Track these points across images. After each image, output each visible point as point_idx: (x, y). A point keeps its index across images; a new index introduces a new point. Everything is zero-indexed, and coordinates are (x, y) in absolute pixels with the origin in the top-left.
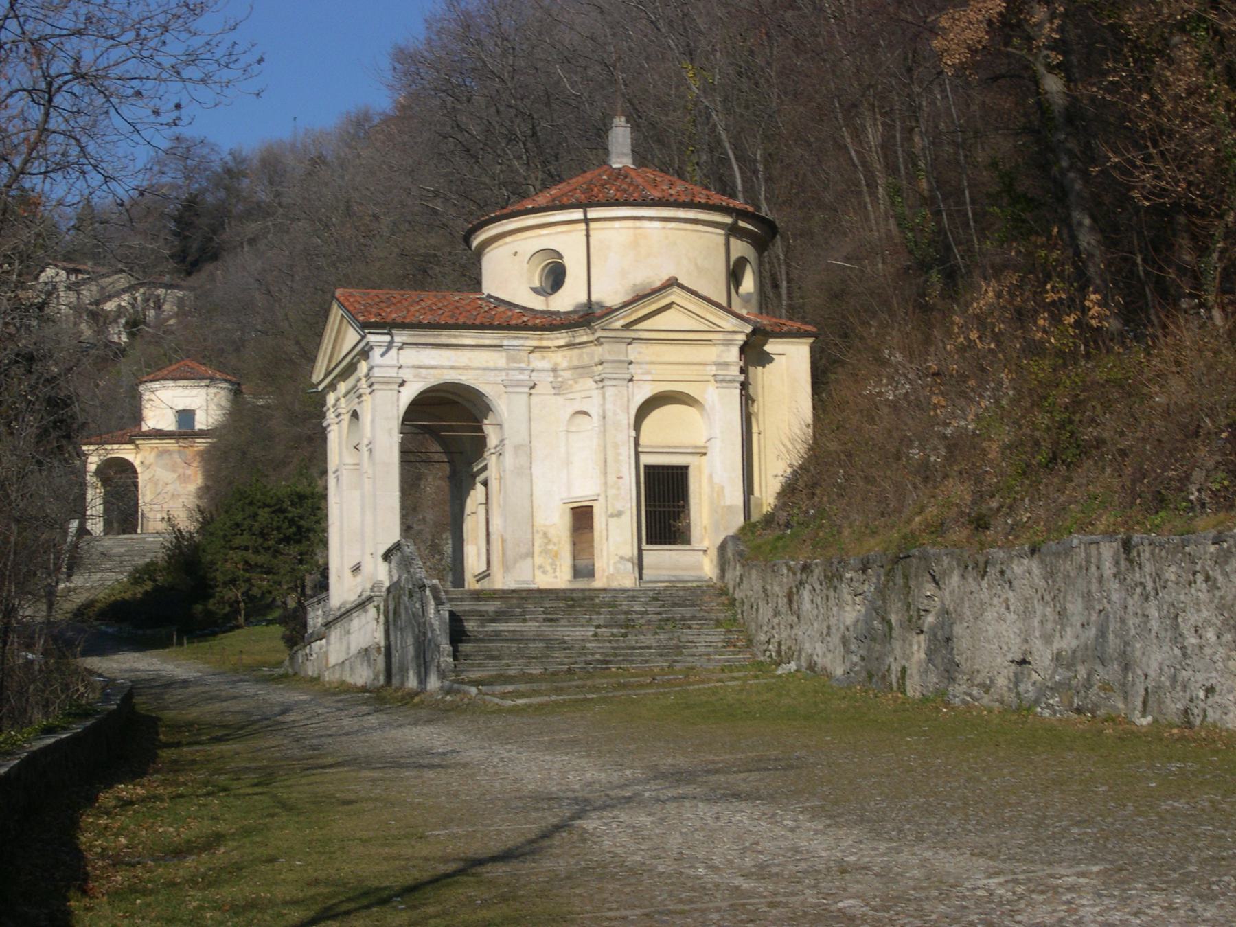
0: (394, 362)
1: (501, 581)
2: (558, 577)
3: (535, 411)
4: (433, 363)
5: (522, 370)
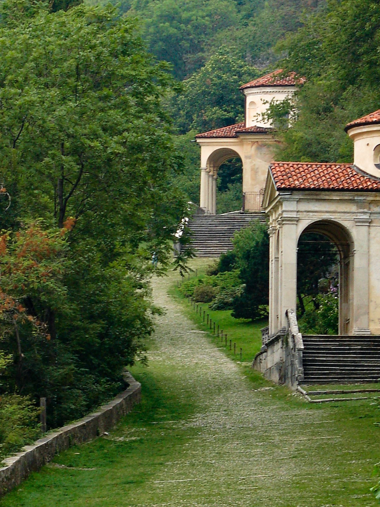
0: (295, 209)
3: (372, 235)
4: (316, 209)
5: (365, 213)
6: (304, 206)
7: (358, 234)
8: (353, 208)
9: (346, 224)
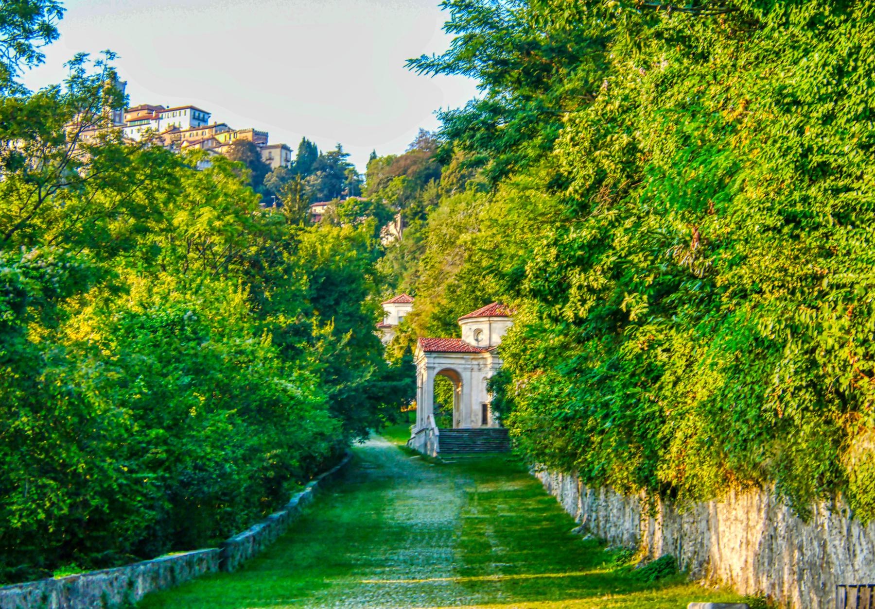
1: (462, 426)
2: (478, 425)
6: (437, 361)
7: (465, 375)
8: (463, 362)
9: (459, 370)
